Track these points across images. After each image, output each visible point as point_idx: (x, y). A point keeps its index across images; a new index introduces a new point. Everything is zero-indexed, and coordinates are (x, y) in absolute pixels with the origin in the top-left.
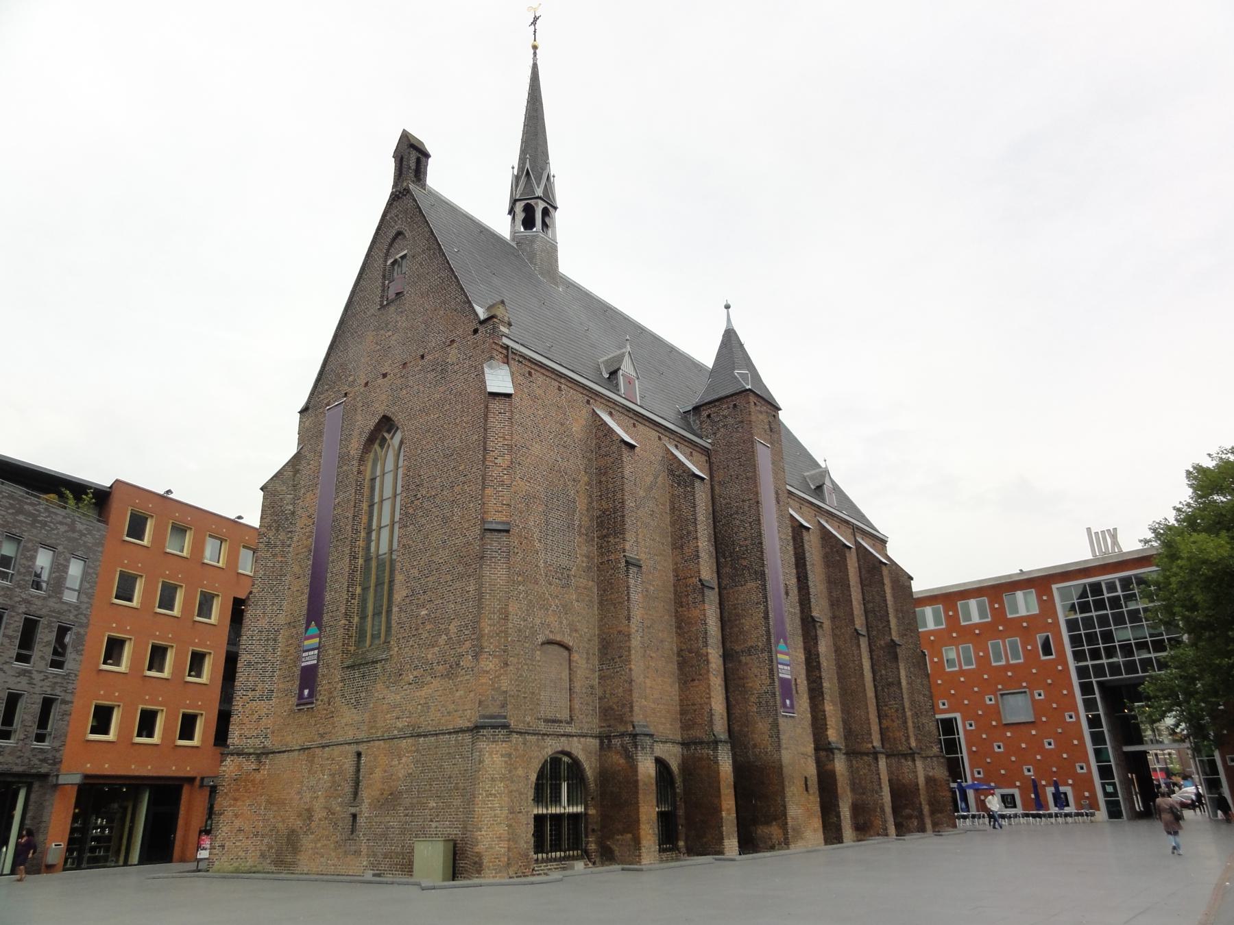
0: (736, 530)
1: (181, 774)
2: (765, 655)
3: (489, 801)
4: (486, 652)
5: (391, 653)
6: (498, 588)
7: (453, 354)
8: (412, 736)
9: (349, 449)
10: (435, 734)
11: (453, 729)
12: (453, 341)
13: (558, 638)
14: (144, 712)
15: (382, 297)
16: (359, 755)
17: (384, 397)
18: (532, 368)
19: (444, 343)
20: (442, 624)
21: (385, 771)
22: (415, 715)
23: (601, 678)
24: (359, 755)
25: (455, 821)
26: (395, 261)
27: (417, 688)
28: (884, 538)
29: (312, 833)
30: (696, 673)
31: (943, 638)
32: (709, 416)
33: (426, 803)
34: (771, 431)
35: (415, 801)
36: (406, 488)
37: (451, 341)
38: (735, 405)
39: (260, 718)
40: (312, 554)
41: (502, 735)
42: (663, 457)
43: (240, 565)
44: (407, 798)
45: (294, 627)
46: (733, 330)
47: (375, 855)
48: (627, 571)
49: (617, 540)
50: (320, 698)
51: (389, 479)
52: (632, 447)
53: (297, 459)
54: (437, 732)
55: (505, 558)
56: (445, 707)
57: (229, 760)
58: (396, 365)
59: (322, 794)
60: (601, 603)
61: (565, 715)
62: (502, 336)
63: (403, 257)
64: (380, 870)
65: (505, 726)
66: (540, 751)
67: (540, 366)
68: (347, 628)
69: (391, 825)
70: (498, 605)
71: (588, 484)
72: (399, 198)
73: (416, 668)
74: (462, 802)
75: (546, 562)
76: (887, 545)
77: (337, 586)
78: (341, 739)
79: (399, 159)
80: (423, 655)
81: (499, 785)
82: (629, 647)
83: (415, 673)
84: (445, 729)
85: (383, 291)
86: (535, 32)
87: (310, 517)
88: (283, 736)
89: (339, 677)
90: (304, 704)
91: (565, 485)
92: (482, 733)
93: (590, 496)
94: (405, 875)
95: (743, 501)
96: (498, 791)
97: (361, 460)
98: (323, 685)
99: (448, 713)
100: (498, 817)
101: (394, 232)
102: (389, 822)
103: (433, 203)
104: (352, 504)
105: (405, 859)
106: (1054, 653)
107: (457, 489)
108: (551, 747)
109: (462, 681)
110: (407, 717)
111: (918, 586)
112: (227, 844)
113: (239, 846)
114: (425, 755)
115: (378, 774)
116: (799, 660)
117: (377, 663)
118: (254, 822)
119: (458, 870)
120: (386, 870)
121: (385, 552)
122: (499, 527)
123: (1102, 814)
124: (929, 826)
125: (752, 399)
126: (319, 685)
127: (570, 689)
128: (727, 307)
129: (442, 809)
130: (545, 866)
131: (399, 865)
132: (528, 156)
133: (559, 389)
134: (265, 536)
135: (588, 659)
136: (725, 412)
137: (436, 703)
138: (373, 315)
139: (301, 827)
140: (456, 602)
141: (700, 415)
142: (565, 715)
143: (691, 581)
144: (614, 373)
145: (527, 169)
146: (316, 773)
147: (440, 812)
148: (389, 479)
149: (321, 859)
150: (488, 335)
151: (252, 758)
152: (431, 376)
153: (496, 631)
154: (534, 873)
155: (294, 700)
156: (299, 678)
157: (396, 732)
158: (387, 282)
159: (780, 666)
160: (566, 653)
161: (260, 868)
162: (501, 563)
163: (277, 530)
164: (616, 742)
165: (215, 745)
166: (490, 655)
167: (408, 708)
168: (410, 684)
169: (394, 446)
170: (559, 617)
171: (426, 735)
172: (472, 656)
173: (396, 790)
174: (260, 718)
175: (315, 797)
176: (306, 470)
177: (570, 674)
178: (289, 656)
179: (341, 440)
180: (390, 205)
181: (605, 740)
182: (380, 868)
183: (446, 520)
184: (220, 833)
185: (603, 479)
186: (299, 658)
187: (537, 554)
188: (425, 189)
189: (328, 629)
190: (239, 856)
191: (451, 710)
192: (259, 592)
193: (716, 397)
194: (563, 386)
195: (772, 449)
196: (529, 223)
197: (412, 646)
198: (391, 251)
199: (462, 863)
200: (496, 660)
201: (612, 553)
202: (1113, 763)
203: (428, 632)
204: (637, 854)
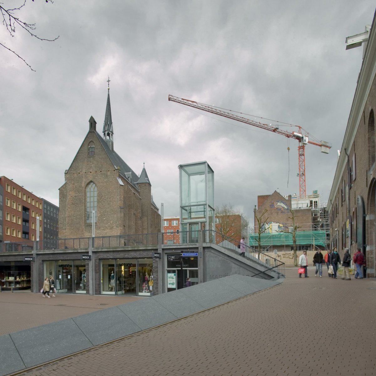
7: (109, 173)
97: (85, 188)
128: (144, 163)
136: (143, 186)
180: (89, 133)
183: (109, 204)
193: (142, 182)
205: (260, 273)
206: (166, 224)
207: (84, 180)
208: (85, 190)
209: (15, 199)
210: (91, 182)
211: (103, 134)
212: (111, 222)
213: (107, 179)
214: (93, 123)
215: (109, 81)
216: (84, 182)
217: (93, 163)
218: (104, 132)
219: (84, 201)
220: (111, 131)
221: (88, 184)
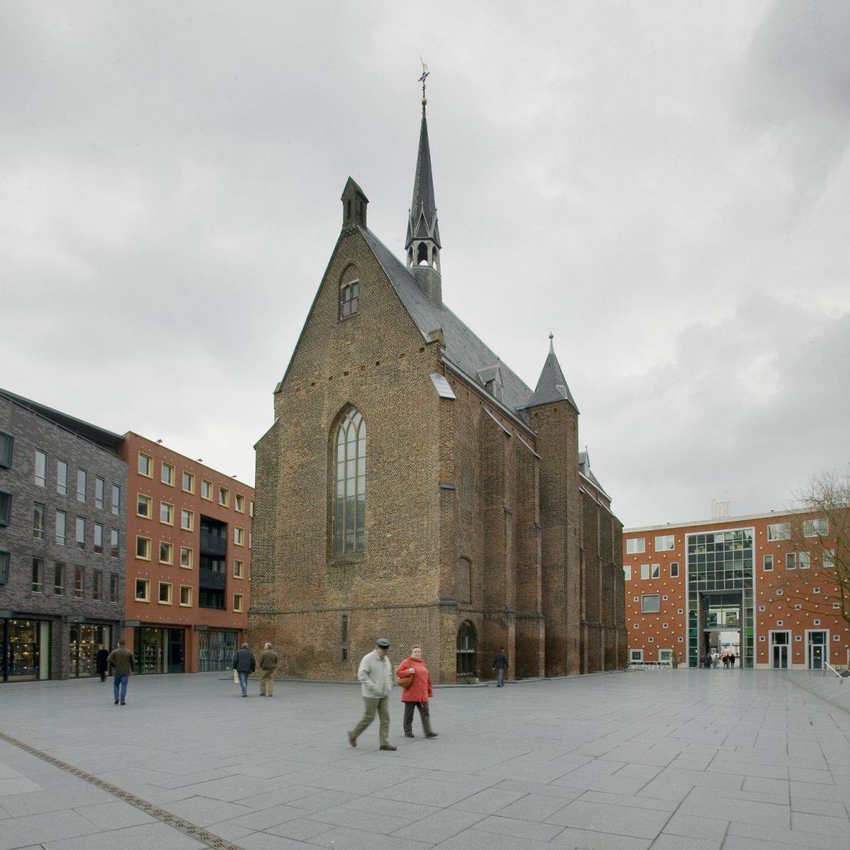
0: (550, 492)
1: (184, 623)
7: (404, 364)
13: (466, 555)
14: (138, 582)
16: (345, 617)
23: (485, 579)
24: (345, 617)
26: (348, 286)
31: (638, 560)
32: (536, 415)
36: (369, 454)
49: (499, 497)
51: (352, 447)
52: (509, 436)
61: (467, 600)
63: (354, 284)
71: (480, 459)
73: (385, 568)
77: (318, 514)
79: (346, 202)
83: (384, 572)
86: (424, 88)
101: (346, 263)
107: (412, 459)
108: (465, 616)
111: (625, 530)
115: (361, 628)
123: (685, 665)
124: (617, 667)
128: (551, 337)
136: (549, 413)
142: (467, 600)
144: (490, 382)
148: (352, 447)
152: (386, 378)
164: (495, 616)
174: (269, 593)
180: (341, 240)
183: (403, 479)
193: (542, 402)
202: (698, 638)
205: (355, 427)
206: (633, 547)
208: (330, 440)
209: (176, 497)
210: (348, 406)
211: (406, 253)
212: (412, 547)
213: (396, 389)
214: (355, 202)
215: (424, 77)
216: (330, 407)
218: (408, 247)
219: (325, 477)
220: (430, 235)
221: (339, 417)
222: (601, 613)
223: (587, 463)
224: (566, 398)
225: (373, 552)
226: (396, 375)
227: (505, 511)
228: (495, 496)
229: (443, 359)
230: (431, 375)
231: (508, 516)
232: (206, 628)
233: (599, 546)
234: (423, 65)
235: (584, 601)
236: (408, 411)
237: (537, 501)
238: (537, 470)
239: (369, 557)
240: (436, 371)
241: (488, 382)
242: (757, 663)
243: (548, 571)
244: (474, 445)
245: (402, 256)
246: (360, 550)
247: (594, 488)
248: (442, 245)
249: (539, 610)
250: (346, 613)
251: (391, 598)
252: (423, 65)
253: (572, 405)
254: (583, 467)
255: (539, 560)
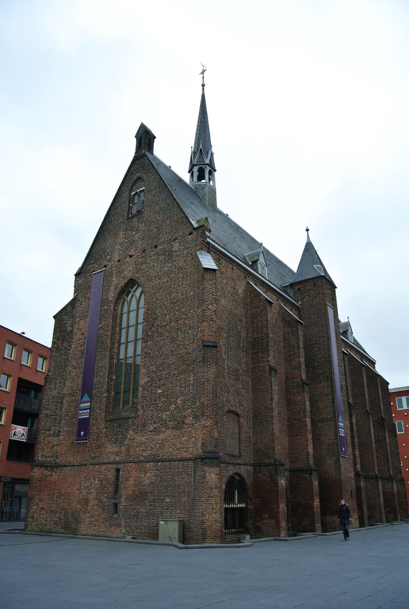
0: (315, 353)
2: (332, 423)
3: (209, 500)
4: (205, 415)
5: (138, 413)
6: (211, 379)
8: (153, 461)
9: (108, 296)
10: (169, 461)
11: (181, 458)
12: (176, 239)
13: (234, 409)
15: (128, 213)
16: (118, 470)
17: (131, 268)
18: (220, 256)
19: (170, 240)
20: (172, 398)
21: (136, 480)
22: (155, 449)
24: (118, 470)
25: (183, 510)
26: (136, 193)
27: (156, 434)
28: (374, 361)
29: (89, 513)
30: (299, 432)
32: (299, 289)
33: (164, 499)
34: (333, 299)
35: (156, 498)
36: (146, 319)
37: (174, 239)
38: (315, 284)
39: (53, 446)
40: (85, 355)
41: (216, 463)
42: (279, 310)
43: (22, 360)
44: (151, 496)
45: (73, 396)
46: (311, 243)
47: (130, 526)
48: (271, 373)
49: (264, 355)
50: (92, 437)
51: (133, 315)
53: (72, 304)
54: (171, 460)
55: (215, 362)
56: (175, 446)
57: (36, 469)
58: (138, 251)
59: (94, 491)
60: (254, 390)
61: (236, 452)
62: (207, 237)
63: (141, 191)
64: (134, 536)
65: (218, 458)
66: (227, 473)
67: (224, 256)
68: (108, 398)
69: (140, 511)
70: (211, 389)
71: (246, 323)
72: (139, 159)
74: (187, 500)
75: (228, 366)
76: (375, 365)
77: (101, 374)
78: (106, 461)
80: (160, 416)
81: (215, 491)
82: (272, 416)
83: (154, 426)
84: (175, 458)
85: (129, 209)
86: (203, 78)
87: (82, 334)
88: (67, 457)
89: (104, 425)
90: (81, 440)
91: (236, 323)
92: (204, 462)
93: (247, 330)
94: (150, 539)
95: (320, 337)
96: (214, 494)
98: (94, 430)
99: (177, 449)
100: (214, 509)
102: (139, 509)
103: (158, 163)
104: (111, 328)
105: (150, 530)
106: (404, 431)
108: (232, 470)
109: (186, 431)
110: (149, 451)
112: (35, 516)
113: (42, 517)
114: (162, 472)
115: (131, 482)
116: (348, 426)
117: (129, 419)
118: (50, 505)
119: (186, 538)
120: (138, 536)
121: (132, 356)
122: (211, 344)
125: (324, 281)
126: (90, 429)
127: (239, 439)
128: (307, 230)
129: (174, 503)
130: (229, 537)
131: (146, 533)
132: (201, 142)
133: (233, 269)
134: (56, 344)
135: (247, 422)
137: (169, 443)
138: (123, 222)
139: (80, 509)
140: (181, 386)
141: (294, 288)
142: (236, 452)
143: (295, 380)
144: (255, 262)
145: (201, 148)
146: (90, 479)
147: (173, 505)
148: (133, 315)
149: (95, 528)
150: (199, 236)
151: (49, 469)
152: (161, 258)
153: (211, 404)
154: (225, 540)
155: (74, 438)
156: (77, 425)
157: (142, 459)
158: (131, 205)
159: (340, 429)
160: (237, 418)
161: (54, 530)
162: (213, 365)
163: (63, 341)
165: (7, 459)
166: (208, 417)
167: (150, 445)
168: (151, 432)
169: (136, 298)
170: (234, 397)
171: (163, 461)
172: (192, 418)
173: (144, 491)
174: (53, 446)
175: (90, 493)
176: (80, 308)
177: (239, 430)
178: (70, 412)
179: (102, 291)
181: (257, 466)
182: (134, 535)
183: (173, 340)
184: (31, 510)
185: (255, 320)
186: (77, 414)
187: (224, 361)
188: (153, 156)
189: (96, 398)
190: (42, 523)
191: (179, 448)
192: (52, 375)
193: (303, 279)
194: (234, 267)
195: (334, 310)
196: (201, 177)
197: (152, 410)
198: (133, 188)
199: (188, 534)
200: (211, 421)
201: (260, 362)
203: (163, 403)
204: (278, 531)
207: (115, 280)
210: (132, 283)
211: (189, 175)
215: (203, 72)
216: (117, 282)
217: (138, 231)
218: (191, 171)
219: (109, 341)
222: (376, 464)
223: (350, 330)
224: (323, 274)
225: (145, 407)
226: (169, 255)
227: (270, 368)
228: (260, 355)
229: (208, 240)
230: (197, 253)
231: (273, 372)
232: (9, 479)
233: (367, 401)
234: (203, 66)
235: (357, 453)
236: (178, 283)
237: (302, 360)
238: (301, 333)
239: (142, 411)
240: (202, 249)
241: (253, 262)
242: (403, 408)
243: (319, 425)
244: (240, 311)
245: (186, 177)
246: (135, 406)
247: (359, 351)
248: (216, 168)
249: (311, 462)
250: (119, 466)
251: (160, 452)
252: (203, 66)
253: (328, 280)
254: (347, 334)
255: (308, 414)
